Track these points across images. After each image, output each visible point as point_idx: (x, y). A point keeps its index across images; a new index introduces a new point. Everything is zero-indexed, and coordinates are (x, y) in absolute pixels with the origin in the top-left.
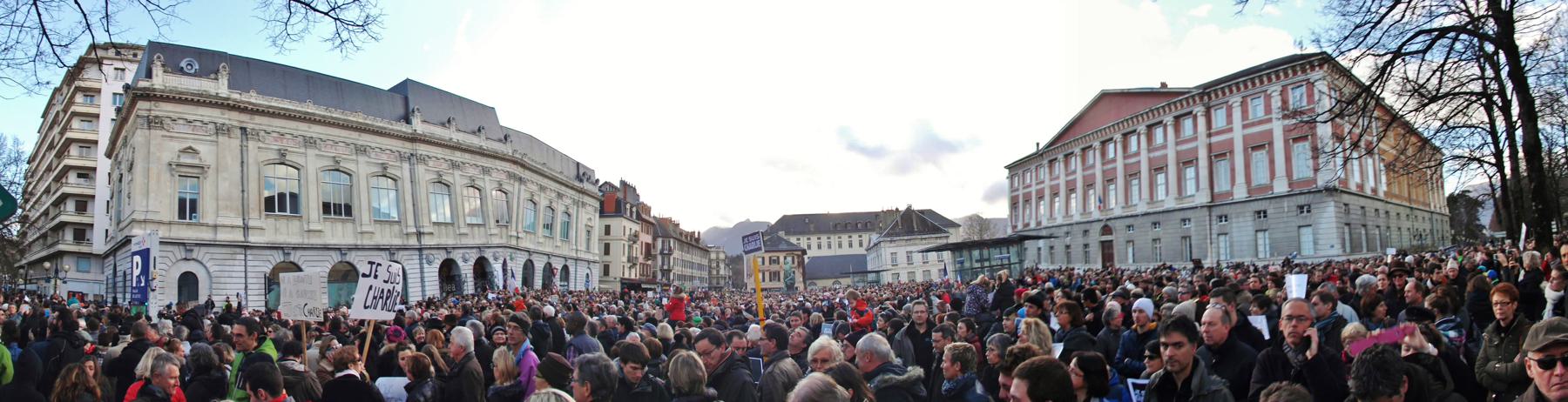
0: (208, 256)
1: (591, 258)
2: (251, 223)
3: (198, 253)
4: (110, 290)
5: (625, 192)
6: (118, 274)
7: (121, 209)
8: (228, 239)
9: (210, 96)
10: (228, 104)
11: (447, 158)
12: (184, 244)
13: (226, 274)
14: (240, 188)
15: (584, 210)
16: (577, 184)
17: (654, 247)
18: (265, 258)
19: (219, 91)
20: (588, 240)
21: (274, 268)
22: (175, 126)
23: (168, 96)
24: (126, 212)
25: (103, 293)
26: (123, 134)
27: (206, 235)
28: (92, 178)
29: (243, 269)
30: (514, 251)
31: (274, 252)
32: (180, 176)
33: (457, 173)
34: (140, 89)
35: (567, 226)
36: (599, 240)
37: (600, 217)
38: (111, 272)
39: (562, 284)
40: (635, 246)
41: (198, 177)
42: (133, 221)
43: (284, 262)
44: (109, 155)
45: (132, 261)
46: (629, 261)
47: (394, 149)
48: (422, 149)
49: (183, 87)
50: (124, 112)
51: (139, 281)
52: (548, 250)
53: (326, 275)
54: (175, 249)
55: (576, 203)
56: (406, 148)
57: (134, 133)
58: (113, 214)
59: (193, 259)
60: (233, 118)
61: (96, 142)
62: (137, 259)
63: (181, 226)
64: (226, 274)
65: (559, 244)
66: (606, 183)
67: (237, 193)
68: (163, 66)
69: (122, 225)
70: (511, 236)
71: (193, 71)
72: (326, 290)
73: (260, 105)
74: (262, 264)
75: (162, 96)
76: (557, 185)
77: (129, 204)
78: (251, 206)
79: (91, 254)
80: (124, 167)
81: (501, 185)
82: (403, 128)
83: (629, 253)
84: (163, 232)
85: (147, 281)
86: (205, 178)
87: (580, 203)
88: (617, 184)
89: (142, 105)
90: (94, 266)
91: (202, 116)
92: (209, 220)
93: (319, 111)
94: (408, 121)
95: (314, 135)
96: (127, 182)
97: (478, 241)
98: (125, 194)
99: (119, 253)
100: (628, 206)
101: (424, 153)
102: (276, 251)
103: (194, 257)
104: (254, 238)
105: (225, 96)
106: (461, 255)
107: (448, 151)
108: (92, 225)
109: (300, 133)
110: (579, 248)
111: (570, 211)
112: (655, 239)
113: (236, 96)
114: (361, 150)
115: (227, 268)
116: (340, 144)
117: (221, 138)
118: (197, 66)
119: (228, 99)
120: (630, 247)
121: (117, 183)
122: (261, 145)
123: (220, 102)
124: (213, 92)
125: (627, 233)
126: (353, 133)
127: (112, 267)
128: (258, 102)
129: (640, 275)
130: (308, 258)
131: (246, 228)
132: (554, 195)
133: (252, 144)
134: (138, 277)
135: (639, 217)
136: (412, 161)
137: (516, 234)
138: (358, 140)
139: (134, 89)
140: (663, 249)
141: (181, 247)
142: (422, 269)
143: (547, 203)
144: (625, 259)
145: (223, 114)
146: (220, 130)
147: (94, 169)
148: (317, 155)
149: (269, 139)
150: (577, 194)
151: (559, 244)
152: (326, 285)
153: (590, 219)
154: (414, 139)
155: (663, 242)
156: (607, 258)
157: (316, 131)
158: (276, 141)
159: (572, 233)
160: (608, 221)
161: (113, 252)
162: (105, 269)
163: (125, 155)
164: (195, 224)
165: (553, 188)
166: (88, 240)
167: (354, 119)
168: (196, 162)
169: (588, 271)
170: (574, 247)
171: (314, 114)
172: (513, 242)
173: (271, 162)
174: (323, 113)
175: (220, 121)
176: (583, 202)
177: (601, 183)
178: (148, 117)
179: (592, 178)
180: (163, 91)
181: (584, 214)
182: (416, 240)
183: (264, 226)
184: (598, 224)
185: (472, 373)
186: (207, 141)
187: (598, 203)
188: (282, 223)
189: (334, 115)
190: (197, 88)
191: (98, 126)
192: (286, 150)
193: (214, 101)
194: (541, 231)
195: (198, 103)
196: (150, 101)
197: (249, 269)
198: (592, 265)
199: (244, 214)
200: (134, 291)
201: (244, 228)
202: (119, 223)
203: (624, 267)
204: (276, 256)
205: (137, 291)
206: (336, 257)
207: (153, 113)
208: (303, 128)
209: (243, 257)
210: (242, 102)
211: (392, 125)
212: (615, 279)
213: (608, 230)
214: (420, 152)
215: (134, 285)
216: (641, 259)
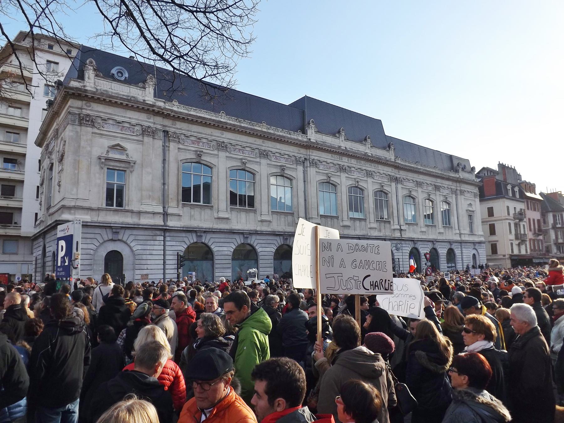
0: (132, 238)
1: (476, 239)
3: (125, 235)
4: (38, 270)
5: (505, 174)
6: (47, 254)
7: (52, 195)
8: (149, 223)
10: (153, 110)
11: (335, 162)
13: (148, 252)
14: (162, 181)
15: (463, 197)
16: (452, 174)
17: (545, 222)
18: (181, 239)
19: (146, 99)
20: (471, 224)
21: (188, 247)
22: (105, 126)
23: (99, 98)
24: (57, 198)
25: (32, 272)
26: (55, 126)
27: (129, 220)
28: (20, 164)
29: (162, 248)
30: (399, 242)
31: (189, 235)
32: (108, 169)
33: (343, 175)
34: (72, 88)
35: (447, 214)
36: (482, 222)
37: (481, 201)
38: (40, 252)
39: (450, 265)
40: (522, 224)
41: (125, 171)
42: (63, 207)
43: (196, 242)
44: (39, 143)
45: (58, 244)
46: (517, 238)
47: (291, 154)
48: (315, 155)
49: (114, 91)
50: (56, 107)
51: (63, 261)
52: (431, 237)
53: (231, 254)
54: (103, 232)
55: (454, 192)
56: (302, 153)
57: (65, 128)
58: (43, 200)
59: (119, 240)
60: (157, 122)
61: (26, 130)
62: (62, 243)
63: (108, 212)
64: (148, 252)
65: (442, 230)
66: (484, 169)
67: (158, 185)
68: (95, 70)
69: (52, 210)
70: (394, 230)
71: (123, 79)
72: (230, 266)
73: (181, 113)
74: (178, 244)
75: (93, 97)
76: (434, 179)
77: (59, 192)
78: (170, 196)
79: (20, 236)
80: (55, 157)
81: (382, 186)
82: (299, 137)
83: (516, 230)
84: (87, 217)
85: (70, 261)
86: (131, 172)
87: (458, 192)
88: (495, 168)
89: (73, 103)
90: (23, 248)
91: (130, 118)
92: (135, 207)
93: (232, 121)
94: (304, 132)
95: (226, 141)
96: (57, 172)
98: (55, 182)
99: (48, 236)
100: (509, 187)
101: (316, 158)
102: (190, 234)
103: (120, 238)
104: (172, 223)
105: (151, 103)
107: (336, 157)
108: (21, 209)
109: (214, 138)
110: (462, 232)
111: (449, 200)
112: (544, 215)
113: (160, 104)
114: (264, 154)
115: (148, 247)
116: (248, 149)
117: (146, 139)
118: (126, 75)
119: (153, 106)
120: (516, 225)
121: (48, 171)
122: (181, 146)
123: (146, 108)
124: (140, 98)
125: (512, 212)
126: (257, 140)
127: (41, 248)
128: (180, 110)
129: (531, 250)
130: (217, 240)
131: (165, 215)
132: (430, 188)
133: (173, 146)
134: (63, 258)
135: (523, 197)
136: (305, 164)
137: (399, 228)
138: (262, 146)
139: (66, 88)
140: (555, 223)
141: (108, 230)
143: (426, 196)
144: (512, 237)
145: (149, 119)
146: (146, 132)
147: (24, 155)
148: (227, 157)
149: (188, 142)
150: (455, 184)
151: (442, 230)
152: (230, 261)
153: (470, 205)
154: (309, 146)
155: (554, 217)
156: (493, 238)
157: (227, 137)
158: (193, 143)
159: (454, 219)
160: (490, 204)
161: (43, 234)
162: (34, 251)
163: (56, 146)
164: (121, 211)
165: (429, 182)
166: (16, 223)
167: (260, 129)
168: (124, 157)
169: (474, 252)
170: (458, 232)
171: (226, 123)
172: (397, 235)
173: (189, 161)
174: (233, 123)
175: (147, 124)
176: (461, 191)
177: (477, 170)
178: (79, 114)
179: (467, 166)
180: (94, 93)
181: (463, 201)
183: (181, 213)
184: (479, 209)
187: (477, 189)
188: (196, 212)
189: (243, 125)
190: (126, 94)
191: (28, 113)
192: (202, 151)
193: (141, 107)
194: (422, 221)
196: (82, 100)
197: (167, 248)
198: (477, 246)
199: (164, 202)
200: (58, 270)
201: (164, 215)
202: (48, 208)
203: (512, 244)
204: (190, 238)
205: (61, 269)
206: (239, 240)
207: (85, 112)
208: (217, 134)
209: (162, 238)
210: (165, 109)
211: (290, 134)
212: (504, 256)
213: (491, 212)
214: (312, 157)
215: (59, 264)
216: (530, 235)
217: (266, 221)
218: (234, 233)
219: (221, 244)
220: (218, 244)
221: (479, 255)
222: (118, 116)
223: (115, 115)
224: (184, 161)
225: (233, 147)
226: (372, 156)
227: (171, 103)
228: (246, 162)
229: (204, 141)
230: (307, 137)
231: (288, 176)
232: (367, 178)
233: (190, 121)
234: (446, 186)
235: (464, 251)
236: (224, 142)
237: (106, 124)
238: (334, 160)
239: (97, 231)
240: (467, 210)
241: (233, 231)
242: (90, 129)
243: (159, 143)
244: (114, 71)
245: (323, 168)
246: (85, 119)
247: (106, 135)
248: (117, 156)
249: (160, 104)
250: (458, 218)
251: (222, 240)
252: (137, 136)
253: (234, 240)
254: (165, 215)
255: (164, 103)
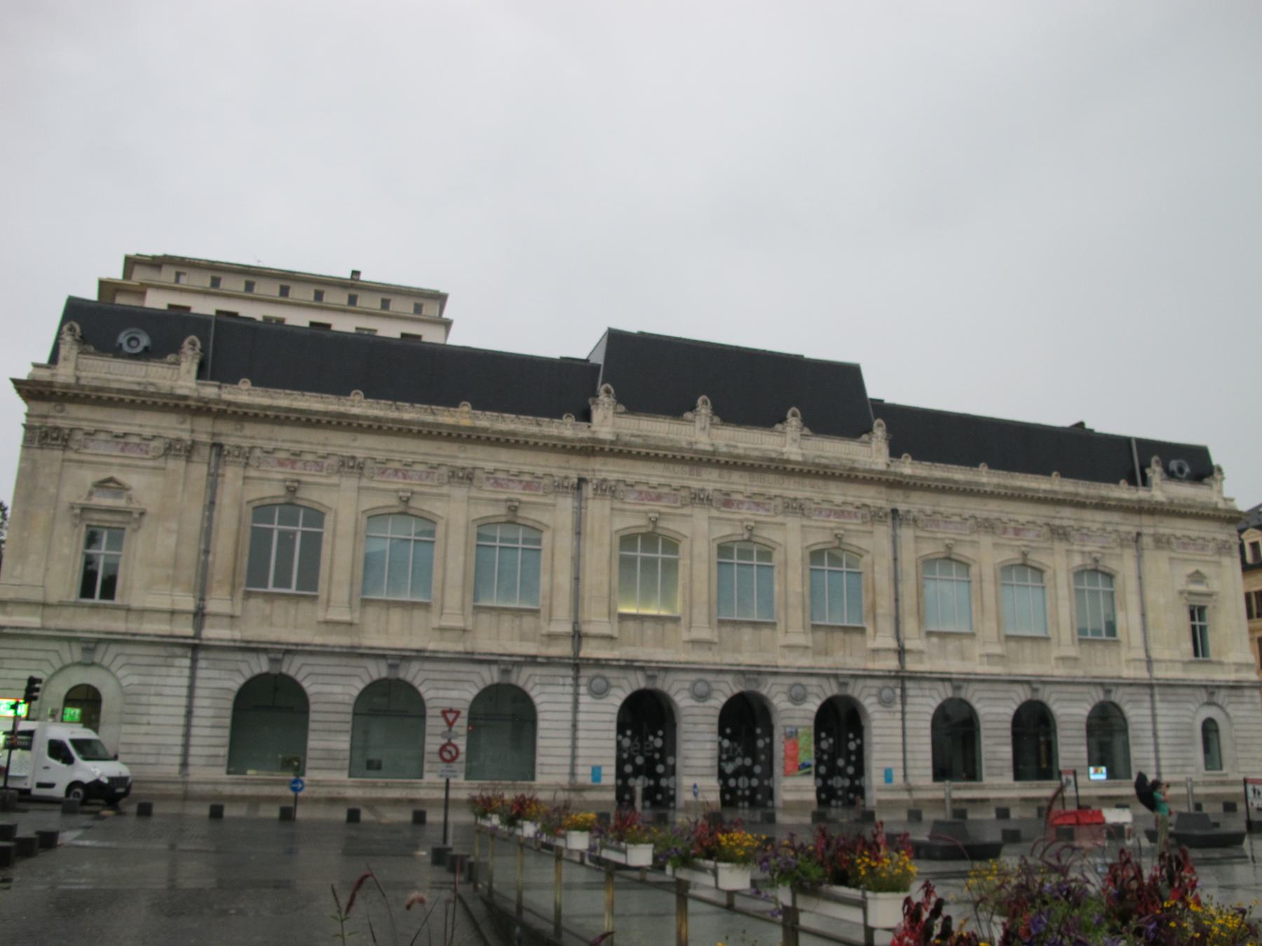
0: (121, 660)
1: (1221, 676)
2: (909, 645)
3: (106, 655)
9: (681, 449)
12: (949, 680)
27: (118, 625)
41: (124, 529)
48: (608, 470)
54: (64, 648)
60: (203, 430)
67: (190, 554)
76: (1044, 512)
82: (567, 428)
86: (135, 531)
87: (1147, 540)
91: (141, 426)
94: (586, 416)
97: (747, 658)
102: (66, 645)
104: (214, 632)
106: (687, 685)
115: (155, 680)
138: (1054, 517)
142: (576, 703)
145: (183, 423)
153: (1197, 577)
154: (591, 449)
168: (121, 503)
178: (40, 428)
182: (1145, 669)
185: (908, 913)
186: (145, 467)
195: (647, 457)
199: (202, 591)
207: (51, 422)
209: (187, 662)
217: (451, 629)
218: (362, 655)
219: (327, 679)
220: (321, 679)
221: (1232, 724)
222: (117, 423)
223: (111, 422)
224: (480, 522)
225: (380, 465)
226: (805, 463)
227: (235, 386)
228: (843, 535)
229: (309, 457)
230: (589, 427)
231: (530, 523)
232: (873, 524)
233: (644, 456)
234: (1095, 527)
235: (1161, 708)
236: (353, 458)
237: (93, 440)
238: (672, 478)
239: (1085, 689)
240: (1181, 593)
241: (1043, 679)
242: (58, 454)
243: (199, 471)
244: (123, 339)
245: (635, 499)
246: (346, 465)
247: (90, 462)
248: (107, 501)
249: (210, 391)
250: (1143, 615)
251: (325, 670)
252: (154, 458)
253: (362, 670)
254: (901, 652)
255: (220, 387)
